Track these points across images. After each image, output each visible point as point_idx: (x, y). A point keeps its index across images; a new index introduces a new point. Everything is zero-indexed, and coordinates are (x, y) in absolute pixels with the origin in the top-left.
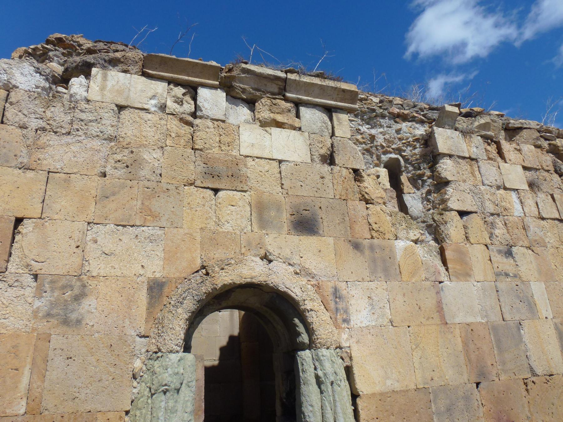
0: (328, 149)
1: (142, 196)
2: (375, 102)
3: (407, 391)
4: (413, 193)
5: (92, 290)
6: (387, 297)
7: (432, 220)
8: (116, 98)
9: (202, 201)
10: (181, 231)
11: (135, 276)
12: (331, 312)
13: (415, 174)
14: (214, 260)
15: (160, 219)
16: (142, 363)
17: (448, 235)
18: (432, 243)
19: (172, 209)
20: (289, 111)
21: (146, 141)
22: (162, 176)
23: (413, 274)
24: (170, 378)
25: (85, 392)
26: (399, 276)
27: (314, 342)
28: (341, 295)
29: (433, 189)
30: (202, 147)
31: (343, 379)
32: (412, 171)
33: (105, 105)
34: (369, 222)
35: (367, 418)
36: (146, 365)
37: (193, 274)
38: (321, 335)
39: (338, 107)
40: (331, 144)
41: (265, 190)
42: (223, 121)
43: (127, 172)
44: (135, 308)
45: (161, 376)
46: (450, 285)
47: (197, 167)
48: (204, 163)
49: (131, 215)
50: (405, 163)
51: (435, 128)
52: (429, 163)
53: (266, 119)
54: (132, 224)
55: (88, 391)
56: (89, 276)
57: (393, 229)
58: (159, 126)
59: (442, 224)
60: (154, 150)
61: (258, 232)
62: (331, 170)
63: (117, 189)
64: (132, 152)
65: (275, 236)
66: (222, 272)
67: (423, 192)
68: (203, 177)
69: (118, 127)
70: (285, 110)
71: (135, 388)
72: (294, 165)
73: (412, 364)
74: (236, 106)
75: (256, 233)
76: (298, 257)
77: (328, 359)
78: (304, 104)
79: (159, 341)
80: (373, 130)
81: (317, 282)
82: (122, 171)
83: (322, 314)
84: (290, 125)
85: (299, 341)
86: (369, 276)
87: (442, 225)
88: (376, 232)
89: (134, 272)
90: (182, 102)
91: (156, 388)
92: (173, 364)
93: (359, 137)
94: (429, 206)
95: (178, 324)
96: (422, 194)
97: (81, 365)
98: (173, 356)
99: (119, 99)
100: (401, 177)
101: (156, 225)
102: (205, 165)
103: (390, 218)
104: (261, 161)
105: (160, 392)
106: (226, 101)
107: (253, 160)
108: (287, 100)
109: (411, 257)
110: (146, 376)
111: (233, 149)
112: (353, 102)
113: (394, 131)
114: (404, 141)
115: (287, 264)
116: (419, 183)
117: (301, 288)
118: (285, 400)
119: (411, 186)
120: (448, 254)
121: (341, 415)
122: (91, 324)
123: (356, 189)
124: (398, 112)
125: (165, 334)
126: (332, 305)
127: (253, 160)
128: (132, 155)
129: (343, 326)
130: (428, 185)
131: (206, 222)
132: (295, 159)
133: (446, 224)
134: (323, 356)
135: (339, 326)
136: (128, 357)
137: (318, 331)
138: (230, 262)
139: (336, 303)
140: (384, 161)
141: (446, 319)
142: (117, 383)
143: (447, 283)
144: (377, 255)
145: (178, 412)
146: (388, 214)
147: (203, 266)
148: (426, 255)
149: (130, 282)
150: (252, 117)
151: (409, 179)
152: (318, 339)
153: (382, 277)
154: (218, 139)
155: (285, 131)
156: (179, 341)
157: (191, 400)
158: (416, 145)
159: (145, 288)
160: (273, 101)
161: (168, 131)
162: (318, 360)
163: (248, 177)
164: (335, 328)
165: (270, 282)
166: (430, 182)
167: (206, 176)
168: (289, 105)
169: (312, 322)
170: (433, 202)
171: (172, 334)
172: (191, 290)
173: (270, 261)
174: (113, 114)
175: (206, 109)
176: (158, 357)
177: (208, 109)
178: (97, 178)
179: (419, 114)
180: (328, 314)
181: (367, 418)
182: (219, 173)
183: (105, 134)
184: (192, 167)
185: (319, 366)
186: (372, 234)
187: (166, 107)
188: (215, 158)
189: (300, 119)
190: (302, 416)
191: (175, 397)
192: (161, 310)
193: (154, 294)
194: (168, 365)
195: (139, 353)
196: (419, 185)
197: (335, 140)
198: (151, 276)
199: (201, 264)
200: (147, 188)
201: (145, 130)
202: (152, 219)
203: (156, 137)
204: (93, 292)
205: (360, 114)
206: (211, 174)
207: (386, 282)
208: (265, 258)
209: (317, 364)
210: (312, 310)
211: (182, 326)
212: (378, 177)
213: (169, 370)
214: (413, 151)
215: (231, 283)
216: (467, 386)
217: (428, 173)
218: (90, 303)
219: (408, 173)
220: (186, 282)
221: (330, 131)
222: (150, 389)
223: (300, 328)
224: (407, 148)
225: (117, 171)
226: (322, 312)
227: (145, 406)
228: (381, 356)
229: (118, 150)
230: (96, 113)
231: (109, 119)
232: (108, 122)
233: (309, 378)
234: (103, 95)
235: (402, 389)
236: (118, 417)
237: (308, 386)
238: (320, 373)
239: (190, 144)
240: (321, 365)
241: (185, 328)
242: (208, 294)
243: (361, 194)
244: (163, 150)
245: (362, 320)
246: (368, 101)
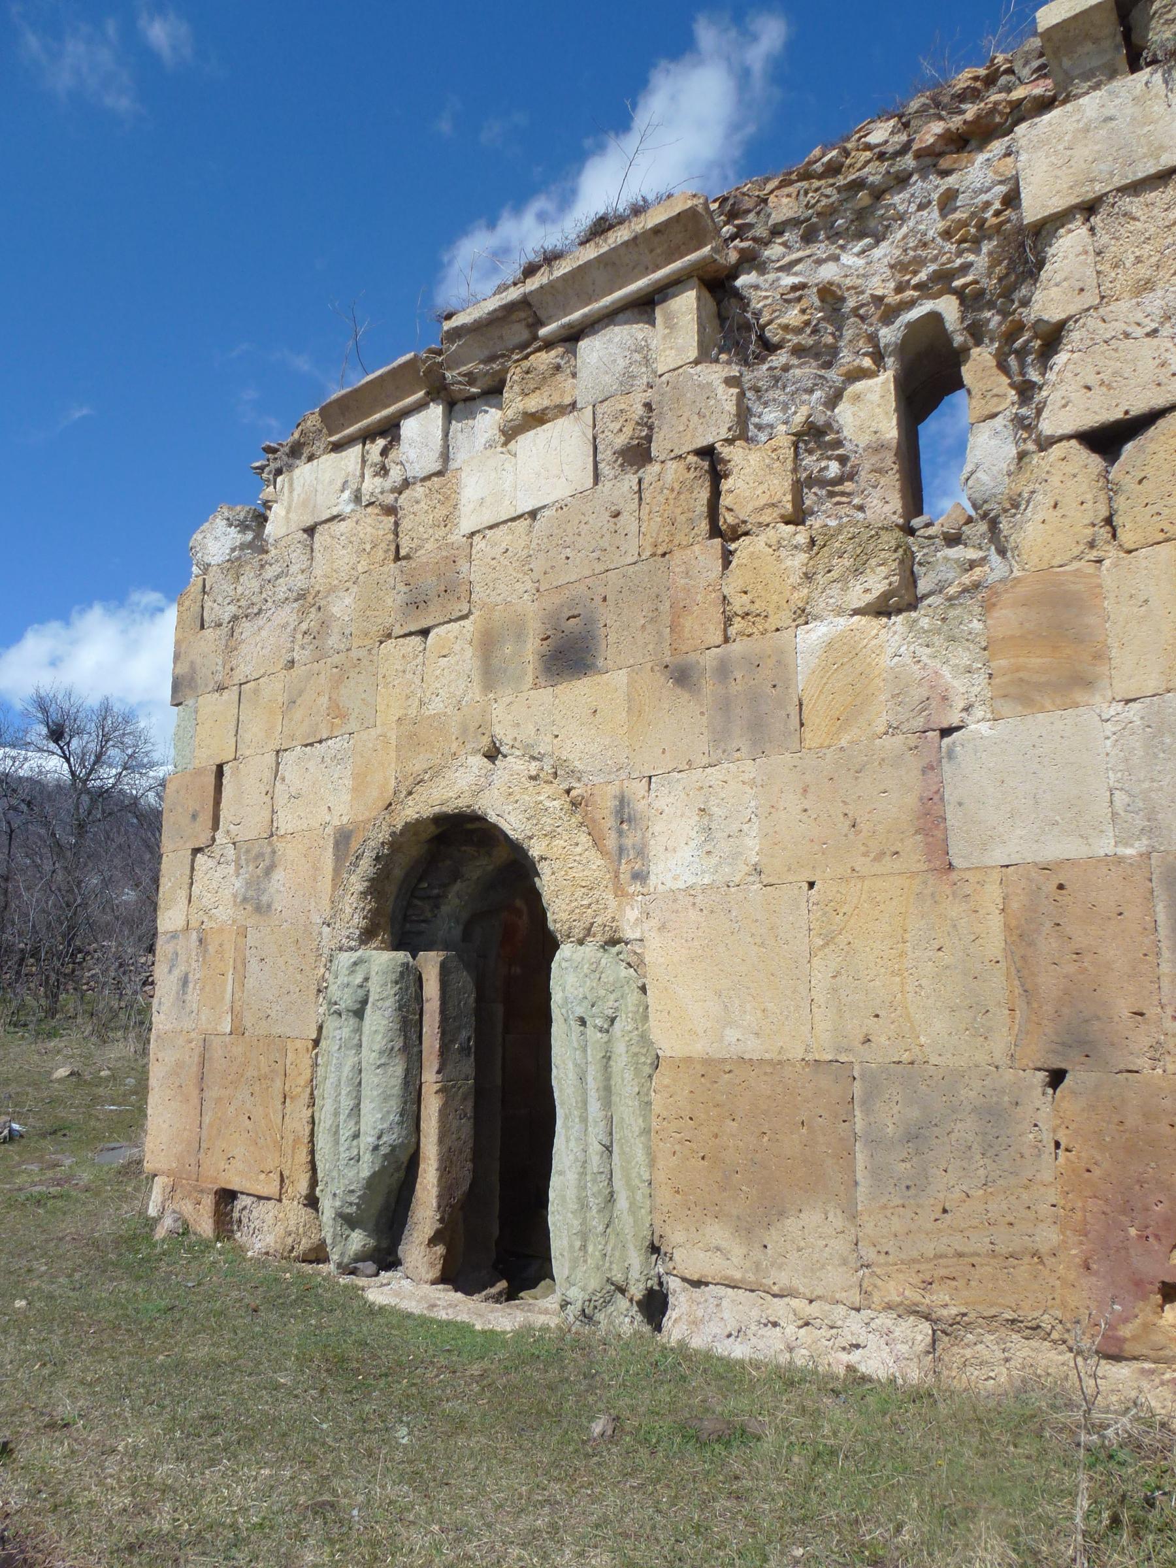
3: (780, 1063)
35: (665, 1114)
39: (662, 284)
65: (507, 700)
88: (743, 618)
109: (846, 667)
129: (631, 889)
139: (620, 833)
153: (743, 749)
205: (821, 225)
216: (1001, 1077)
235: (767, 1056)
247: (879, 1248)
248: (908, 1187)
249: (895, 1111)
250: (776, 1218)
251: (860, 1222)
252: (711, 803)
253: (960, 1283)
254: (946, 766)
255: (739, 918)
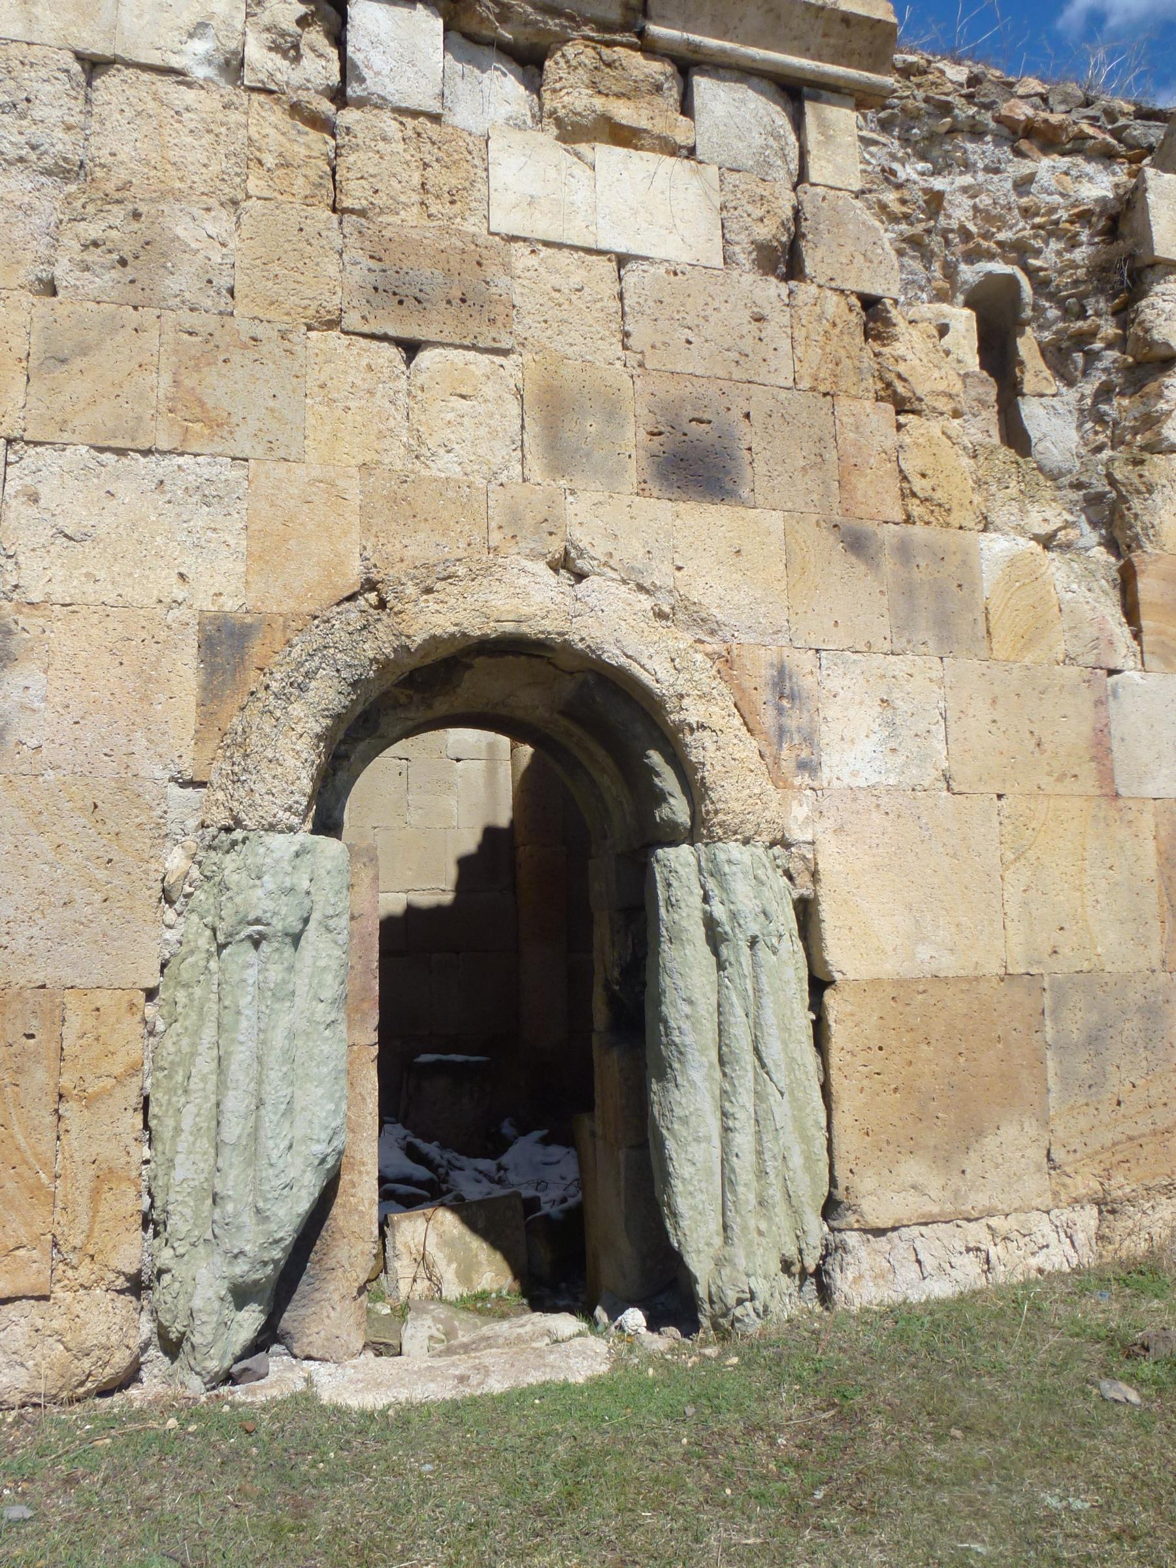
0: (783, 224)
1: (174, 358)
2: (951, 81)
3: (977, 979)
4: (1054, 396)
5: (30, 644)
6: (941, 704)
7: (1105, 482)
8: (74, 29)
9: (364, 380)
10: (299, 470)
11: (158, 606)
12: (763, 737)
13: (1065, 330)
14: (404, 565)
15: (231, 433)
16: (187, 857)
17: (1153, 527)
18: (1100, 554)
19: (271, 403)
20: (658, 88)
21: (181, 179)
22: (236, 294)
23: (1029, 639)
24: (269, 902)
25: (28, 934)
26: (985, 643)
27: (704, 822)
28: (796, 688)
29: (1120, 381)
30: (364, 202)
31: (788, 935)
32: (1055, 321)
33: (40, 54)
34: (901, 471)
35: (849, 1046)
36: (200, 863)
37: (338, 604)
38: (726, 802)
40: (794, 207)
41: (570, 351)
42: (436, 118)
43: (123, 281)
44: (163, 699)
45: (242, 896)
46: (1141, 681)
47: (349, 268)
48: (372, 257)
49: (139, 419)
50: (1035, 294)
51: (1150, 172)
52: (1115, 296)
53: (579, 114)
54: (147, 446)
55: (35, 931)
56: (21, 603)
57: (977, 499)
58: (223, 130)
59: (1139, 492)
60: (208, 210)
61: (545, 484)
62: (789, 296)
63: (92, 336)
64: (136, 215)
65: (598, 497)
66: (427, 601)
67: (1087, 392)
68: (368, 302)
69: (88, 132)
70: (644, 87)
71: (170, 927)
72: (667, 272)
73: (998, 907)
74: (478, 68)
75: (537, 487)
76: (667, 568)
77: (745, 873)
78: (708, 68)
79: (236, 796)
80: (940, 179)
81: (725, 646)
82: (107, 277)
83: (735, 741)
84: (659, 137)
85: (661, 818)
86: (889, 638)
87: (1135, 496)
89: (155, 592)
90: (296, 47)
91: (230, 929)
92: (277, 861)
93: (890, 197)
94: (1101, 438)
95: (293, 750)
96: (1083, 397)
97: (10, 859)
98: (280, 843)
99: (84, 35)
100: (1020, 341)
101: (219, 449)
102: (373, 264)
103: (972, 461)
104: (559, 256)
105: (242, 941)
106: (445, 49)
107: (533, 252)
108: (649, 48)
109: (1028, 588)
110: (200, 895)
111: (467, 213)
112: (878, 60)
113: (1009, 185)
114: (1037, 220)
115: (632, 585)
116: (1074, 362)
117: (673, 660)
118: (617, 988)
119: (1047, 373)
120: (1147, 587)
121: (774, 1031)
122: (34, 743)
123: (868, 362)
124: (1028, 118)
125: (254, 777)
126: (768, 718)
127: (533, 252)
128: (135, 226)
129: (797, 781)
130: (1105, 370)
131: (377, 447)
132: (672, 255)
133: (1150, 492)
134: (729, 862)
135: (785, 781)
136: (146, 840)
137: (720, 789)
138: (452, 569)
139: (780, 711)
140: (965, 282)
141: (1117, 781)
142: (118, 912)
143: (1132, 675)
144: (917, 575)
145: (296, 999)
146: (965, 448)
147: (368, 580)
148: (1074, 586)
149: (144, 624)
150: (531, 109)
151: (1044, 350)
152: (716, 812)
153: (930, 643)
154: (416, 180)
155: (642, 158)
156: (297, 797)
157: (335, 967)
158: (1077, 234)
159: (191, 641)
160: (606, 52)
161: (250, 146)
162: (716, 873)
163: (514, 306)
164: (770, 787)
165: (577, 638)
166: (1111, 360)
167: (377, 299)
168: (657, 69)
169: (700, 763)
170: (1116, 423)
171: (274, 777)
172: (332, 651)
173: (580, 576)
174: (68, 86)
175: (378, 74)
176: (234, 843)
177: (384, 72)
178: (26, 298)
179: (1099, 127)
180: (755, 743)
181: (850, 1045)
182: (421, 291)
183: (46, 152)
184: (332, 270)
185: (716, 892)
186: (910, 508)
187: (242, 64)
188: (406, 240)
189: (692, 118)
190: (662, 1028)
191: (286, 955)
192: (242, 709)
193: (218, 660)
194: (263, 865)
195: (180, 831)
196: (1076, 369)
197: (809, 194)
198: (209, 606)
199: (364, 576)
200: (190, 334)
201: (176, 141)
202: (206, 432)
203: (215, 168)
204: (32, 650)
205: (898, 121)
206: (395, 294)
207: (941, 658)
208: (563, 567)
209: (711, 884)
210: (702, 727)
211: (305, 755)
212: (943, 330)
213: (266, 878)
214: (1067, 256)
215: (453, 635)
217: (1109, 329)
218: (26, 683)
219: (1041, 328)
220: (317, 627)
221: (794, 166)
222: (214, 930)
223: (665, 780)
224: (1047, 245)
225: (91, 278)
226: (736, 736)
227: (202, 978)
228: (906, 876)
229: (91, 209)
230: (12, 82)
231: (56, 104)
232: (53, 115)
233: (684, 923)
234: (31, 20)
235: (962, 973)
236: (125, 1005)
237: (682, 945)
238: (719, 911)
239: (324, 192)
240: (722, 887)
241: (313, 762)
242: (384, 666)
243: (881, 379)
244: (239, 212)
245: (857, 767)
246: (930, 76)
247: (1068, 1148)
248: (1090, 1087)
249: (1078, 1017)
250: (973, 1139)
251: (1052, 1127)
252: (894, 695)
253: (1132, 1164)
254: (1112, 703)
255: (930, 826)
